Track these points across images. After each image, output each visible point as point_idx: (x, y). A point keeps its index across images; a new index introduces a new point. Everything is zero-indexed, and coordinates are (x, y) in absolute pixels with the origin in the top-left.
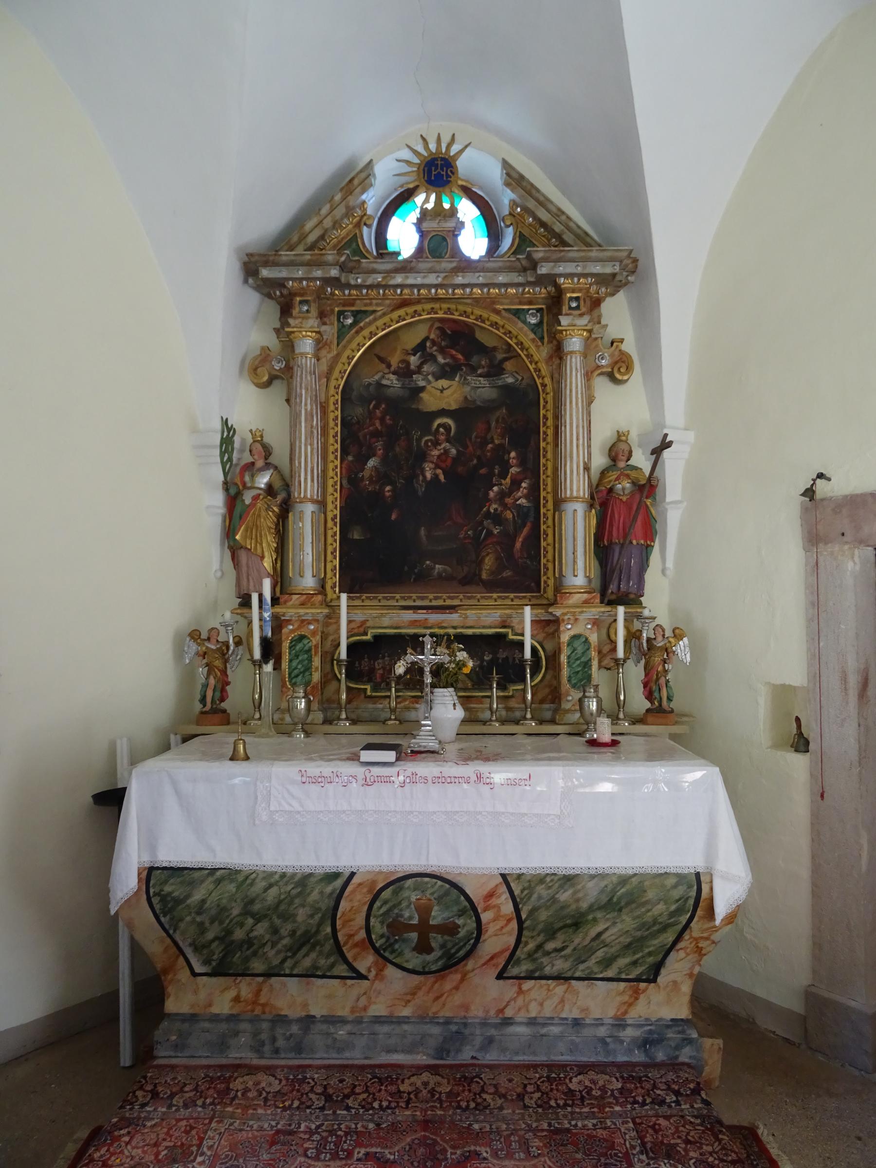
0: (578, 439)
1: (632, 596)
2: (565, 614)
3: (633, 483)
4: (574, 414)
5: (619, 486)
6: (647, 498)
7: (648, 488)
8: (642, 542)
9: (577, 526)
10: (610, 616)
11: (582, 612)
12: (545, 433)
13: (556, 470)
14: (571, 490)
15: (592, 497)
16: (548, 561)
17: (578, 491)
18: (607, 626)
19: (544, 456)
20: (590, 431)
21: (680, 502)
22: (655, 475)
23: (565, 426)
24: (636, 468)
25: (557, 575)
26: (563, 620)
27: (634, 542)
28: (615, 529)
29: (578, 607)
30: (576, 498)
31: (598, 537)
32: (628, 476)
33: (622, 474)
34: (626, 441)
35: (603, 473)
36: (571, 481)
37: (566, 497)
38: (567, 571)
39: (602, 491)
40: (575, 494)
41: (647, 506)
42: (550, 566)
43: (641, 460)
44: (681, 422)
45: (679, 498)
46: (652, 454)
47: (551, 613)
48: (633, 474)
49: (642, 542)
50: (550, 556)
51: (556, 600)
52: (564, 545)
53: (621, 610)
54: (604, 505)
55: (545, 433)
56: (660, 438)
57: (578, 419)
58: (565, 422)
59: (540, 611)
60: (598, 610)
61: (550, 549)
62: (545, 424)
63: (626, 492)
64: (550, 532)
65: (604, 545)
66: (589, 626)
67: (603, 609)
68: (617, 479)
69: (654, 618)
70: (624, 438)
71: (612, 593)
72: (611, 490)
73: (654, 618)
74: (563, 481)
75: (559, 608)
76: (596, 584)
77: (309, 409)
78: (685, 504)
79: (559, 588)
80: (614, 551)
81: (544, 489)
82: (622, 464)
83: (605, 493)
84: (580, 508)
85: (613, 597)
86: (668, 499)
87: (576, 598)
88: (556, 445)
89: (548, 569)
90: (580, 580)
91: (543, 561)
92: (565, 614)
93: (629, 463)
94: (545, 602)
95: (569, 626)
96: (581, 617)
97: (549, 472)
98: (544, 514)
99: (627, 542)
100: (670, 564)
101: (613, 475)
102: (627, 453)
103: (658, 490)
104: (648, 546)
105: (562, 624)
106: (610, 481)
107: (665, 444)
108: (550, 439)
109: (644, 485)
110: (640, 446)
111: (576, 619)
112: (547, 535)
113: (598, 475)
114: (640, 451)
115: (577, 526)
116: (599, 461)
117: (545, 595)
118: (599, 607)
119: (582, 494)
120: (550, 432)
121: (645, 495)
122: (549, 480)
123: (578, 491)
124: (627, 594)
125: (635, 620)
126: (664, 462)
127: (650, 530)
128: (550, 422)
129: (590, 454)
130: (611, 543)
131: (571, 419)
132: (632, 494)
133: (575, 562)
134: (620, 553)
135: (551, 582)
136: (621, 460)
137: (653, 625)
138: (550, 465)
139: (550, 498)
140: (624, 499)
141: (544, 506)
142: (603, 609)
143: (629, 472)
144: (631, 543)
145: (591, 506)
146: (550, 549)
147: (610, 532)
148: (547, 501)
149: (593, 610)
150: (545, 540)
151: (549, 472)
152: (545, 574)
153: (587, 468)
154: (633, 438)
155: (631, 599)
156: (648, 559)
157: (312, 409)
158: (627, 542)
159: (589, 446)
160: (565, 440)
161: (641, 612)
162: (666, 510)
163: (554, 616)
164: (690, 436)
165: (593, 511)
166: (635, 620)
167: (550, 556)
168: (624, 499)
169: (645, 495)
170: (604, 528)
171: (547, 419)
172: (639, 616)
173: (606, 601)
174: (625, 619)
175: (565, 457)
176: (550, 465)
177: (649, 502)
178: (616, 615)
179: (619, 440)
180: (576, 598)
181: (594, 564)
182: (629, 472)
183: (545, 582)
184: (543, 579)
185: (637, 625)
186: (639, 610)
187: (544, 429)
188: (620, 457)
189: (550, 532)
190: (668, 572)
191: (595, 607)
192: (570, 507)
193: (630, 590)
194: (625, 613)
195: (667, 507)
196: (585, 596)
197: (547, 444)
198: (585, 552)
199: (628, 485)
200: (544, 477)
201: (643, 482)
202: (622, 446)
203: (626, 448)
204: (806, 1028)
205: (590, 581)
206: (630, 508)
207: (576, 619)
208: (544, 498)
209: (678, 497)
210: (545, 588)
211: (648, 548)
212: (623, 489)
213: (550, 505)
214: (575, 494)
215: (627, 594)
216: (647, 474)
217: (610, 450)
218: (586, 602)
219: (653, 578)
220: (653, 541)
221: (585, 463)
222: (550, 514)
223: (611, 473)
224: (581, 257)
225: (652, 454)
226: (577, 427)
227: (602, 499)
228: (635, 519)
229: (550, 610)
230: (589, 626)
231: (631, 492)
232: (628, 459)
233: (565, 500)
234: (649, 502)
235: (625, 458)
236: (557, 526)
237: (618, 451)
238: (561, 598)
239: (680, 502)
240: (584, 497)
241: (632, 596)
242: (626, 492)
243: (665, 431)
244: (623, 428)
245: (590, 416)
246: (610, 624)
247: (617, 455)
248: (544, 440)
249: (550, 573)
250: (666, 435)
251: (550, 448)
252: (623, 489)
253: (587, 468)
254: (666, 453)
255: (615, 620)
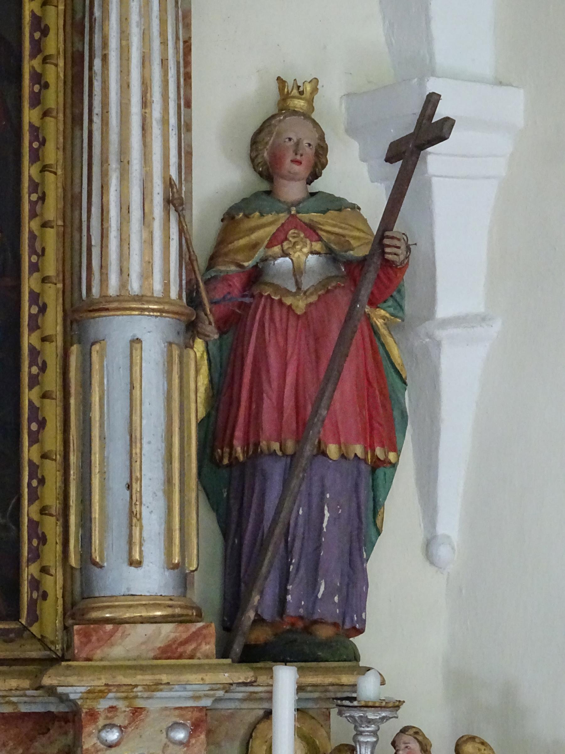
0: (145, 103)
1: (324, 632)
2: (100, 694)
3: (332, 255)
4: (134, 17)
5: (284, 263)
6: (373, 303)
7: (378, 270)
8: (359, 449)
9: (140, 392)
10: (250, 698)
11: (157, 686)
12: (37, 78)
13: (72, 201)
14: (123, 272)
15: (193, 300)
16: (43, 511)
17: (146, 275)
18: (242, 731)
19: (35, 156)
20: (187, 77)
21: (483, 319)
22: (398, 227)
23: (105, 58)
24: (336, 204)
25: (73, 561)
26: (93, 715)
27: (333, 450)
28: (268, 406)
29: (142, 669)
30: (139, 298)
31: (213, 436)
32: (312, 230)
33: (293, 222)
34: (307, 116)
35: (232, 219)
36: (124, 241)
37: (105, 297)
38: (109, 546)
39: (226, 278)
40: (135, 286)
41: (373, 330)
42: (52, 528)
43: (356, 177)
44: (484, 61)
45: (481, 309)
46: (390, 159)
47: (51, 691)
48: (328, 223)
49: (359, 449)
50: (51, 495)
51: (69, 645)
52: (96, 458)
53: (286, 678)
54: (233, 323)
55: (37, 78)
56: (417, 108)
57: (145, 36)
58: (105, 45)
59: (13, 683)
60: (207, 681)
61: (52, 470)
62: (37, 48)
63: (307, 283)
64: (52, 411)
65: (234, 460)
66: (181, 735)
67: (225, 677)
68: (277, 239)
69: (397, 706)
70: (299, 104)
71: (259, 620)
72: (255, 276)
73: (397, 706)
74: (95, 240)
75: (79, 671)
76: (208, 589)
77: (77, 213)
78: (497, 326)
79: (80, 605)
80: (265, 478)
81: (34, 268)
82: (292, 191)
83: (237, 283)
84: (151, 333)
85: (262, 635)
86: (443, 311)
87: (136, 641)
88: (76, 120)
89: (43, 539)
90: (150, 579)
91: (29, 511)
92: (100, 694)
93: (318, 185)
94: (34, 652)
95: (113, 736)
96: (153, 705)
97: (51, 210)
98: (34, 353)
99: (308, 450)
100: (449, 524)
101: (264, 226)
102: (309, 152)
103: (410, 280)
104: (377, 464)
105: (89, 729)
106: (255, 246)
107: (430, 130)
108: (53, 98)
109: (363, 262)
110: (352, 130)
111: (137, 712)
112: (42, 424)
113: (214, 225)
114: (355, 147)
115: (140, 392)
116: (219, 177)
117: (34, 629)
118: (212, 668)
119: (157, 287)
120: (54, 74)
121: (365, 294)
122: (51, 235)
123: (146, 275)
124: (310, 624)
125: (334, 712)
126: (428, 185)
127: (383, 412)
128: (54, 44)
129: (186, 154)
130: (255, 454)
131: (124, 35)
132: (325, 289)
133: (133, 516)
134: (286, 483)
135: (54, 584)
136: (293, 178)
137: (391, 729)
138: (53, 186)
139: (52, 295)
140: (300, 305)
141: (34, 326)
142: (225, 677)
143: (315, 217)
144: (324, 454)
145: (191, 329)
146: (52, 470)
147: (254, 418)
148: (43, 309)
149: (193, 678)
150: (34, 439)
151: (51, 210)
152: (35, 555)
153: (176, 201)
154: (331, 107)
155: (321, 641)
156: (376, 508)
157: (72, 211)
158: (308, 450)
159: (185, 127)
160: (105, 104)
161: (354, 687)
162: (438, 344)
163: (63, 699)
164: (513, 105)
165: (199, 345)
166: (334, 712)
167: (51, 495)
168: (300, 305)
169: (365, 294)
170: (233, 403)
171: (45, 32)
172: (347, 700)
173: (237, 648)
174: (300, 711)
175: (104, 161)
176: (53, 186)
177: (380, 316)
178: (269, 696)
179: (284, 108)
180: (136, 641)
181: (203, 525)
182: (315, 217)
183: (35, 584)
184: (29, 571)
185: (340, 729)
186: (346, 679)
187: (36, 63)
188: (288, 166)
189: (52, 411)
190: (443, 552)
191: (199, 668)
192: (117, 331)
193: (319, 613)
194: (300, 688)
195: (441, 334)
196: (168, 631)
197: (46, 114)
198: (169, 481)
199: (312, 260)
200: (35, 225)
201: (360, 251)
202: (294, 131)
203: (308, 138)
204: (57, 101)
205: (185, 581)
206: (318, 339)
207: (137, 712)
208: (35, 297)
209: (475, 304)
210: (33, 604)
211: (375, 474)
212: (297, 272)
213: (53, 322)
214: (135, 286)
215: (310, 624)
216: (375, 225)
217: (255, 141)
218: (169, 652)
219: (393, 569)
220: (395, 448)
221: (169, 184)
222: (52, 354)
223: (255, 219)
224: (99, 387)
225: (390, 159)
226: (145, 61)
227: (224, 304)
228: (332, 376)
229: (47, 681)
230: (181, 735)
231: (323, 284)
232: (315, 175)
233: (101, 307)
234: (380, 316)
235: (302, 170)
236: (75, 393)
237: (281, 144)
238: (87, 635)
239: (483, 319)
240: (165, 299)
241: (324, 632)
242: (307, 283)
243: (433, 86)
244: (300, 72)
245: (187, 26)
246: (254, 727)
247: (276, 159)
248: (36, 100)
249: (51, 553)
250: (432, 100)
251: (53, 129)
252: (297, 272)
253: (176, 201)
254: (436, 158)
255: (268, 714)
